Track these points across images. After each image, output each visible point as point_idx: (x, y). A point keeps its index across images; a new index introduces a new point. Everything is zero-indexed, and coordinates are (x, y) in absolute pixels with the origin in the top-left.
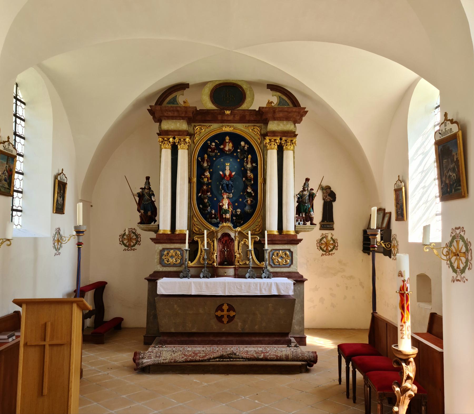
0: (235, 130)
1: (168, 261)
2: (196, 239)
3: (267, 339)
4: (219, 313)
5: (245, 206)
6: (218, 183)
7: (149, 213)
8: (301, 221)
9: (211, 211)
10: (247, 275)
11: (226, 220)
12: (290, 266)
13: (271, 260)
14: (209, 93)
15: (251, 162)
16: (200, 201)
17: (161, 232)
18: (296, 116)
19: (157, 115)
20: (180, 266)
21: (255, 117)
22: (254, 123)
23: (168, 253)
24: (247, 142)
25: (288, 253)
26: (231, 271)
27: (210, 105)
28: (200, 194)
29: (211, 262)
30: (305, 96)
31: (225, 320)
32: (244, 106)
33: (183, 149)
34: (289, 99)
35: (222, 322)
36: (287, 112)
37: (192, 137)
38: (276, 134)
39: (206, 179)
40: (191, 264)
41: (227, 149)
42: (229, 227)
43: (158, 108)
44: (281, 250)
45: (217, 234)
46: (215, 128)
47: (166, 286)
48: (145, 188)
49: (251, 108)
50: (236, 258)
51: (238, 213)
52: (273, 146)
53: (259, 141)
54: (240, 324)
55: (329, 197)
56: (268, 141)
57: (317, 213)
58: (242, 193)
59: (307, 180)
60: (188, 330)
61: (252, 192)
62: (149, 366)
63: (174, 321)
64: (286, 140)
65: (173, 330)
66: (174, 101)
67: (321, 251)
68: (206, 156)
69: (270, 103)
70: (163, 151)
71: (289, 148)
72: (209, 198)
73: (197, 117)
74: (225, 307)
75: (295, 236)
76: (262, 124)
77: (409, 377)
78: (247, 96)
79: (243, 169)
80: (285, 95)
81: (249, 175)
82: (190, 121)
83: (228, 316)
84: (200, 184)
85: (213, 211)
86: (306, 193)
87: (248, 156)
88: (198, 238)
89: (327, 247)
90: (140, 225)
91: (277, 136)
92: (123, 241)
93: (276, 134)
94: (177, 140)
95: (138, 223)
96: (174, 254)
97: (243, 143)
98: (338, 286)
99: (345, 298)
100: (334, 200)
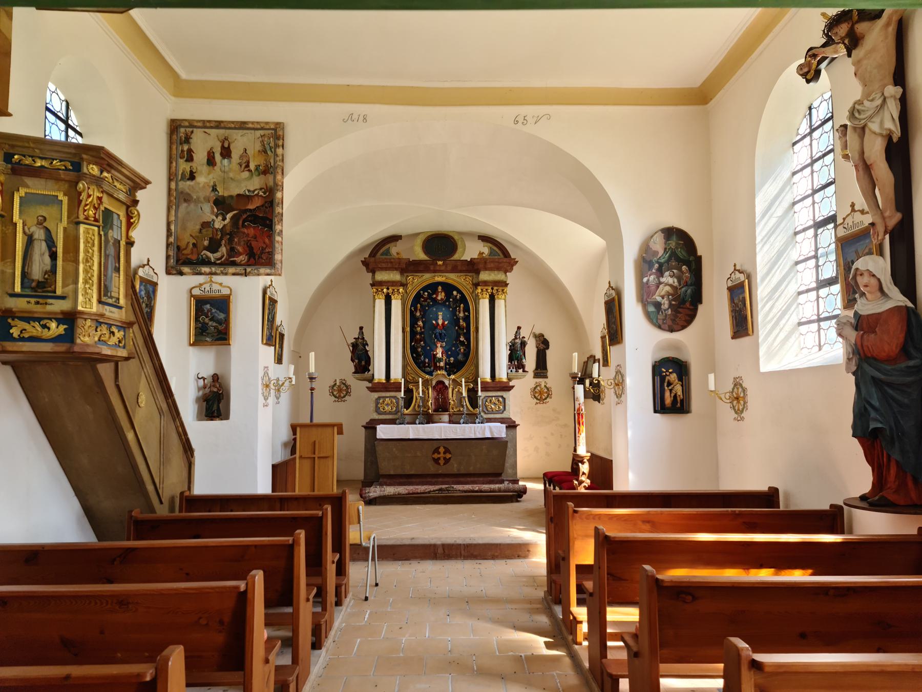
2: (411, 387)
4: (436, 456)
7: (363, 363)
11: (440, 368)
16: (413, 350)
19: (371, 267)
24: (459, 291)
26: (446, 417)
27: (422, 256)
30: (517, 246)
31: (442, 462)
32: (456, 257)
35: (439, 464)
40: (406, 412)
41: (439, 298)
43: (372, 259)
46: (428, 278)
47: (384, 432)
57: (530, 361)
59: (519, 328)
62: (375, 498)
65: (392, 473)
66: (387, 252)
69: (481, 254)
70: (377, 301)
74: (442, 450)
75: (508, 383)
77: (584, 473)
82: (403, 271)
83: (445, 458)
84: (413, 333)
86: (518, 341)
87: (460, 304)
89: (541, 395)
94: (390, 291)
97: (455, 293)
98: (552, 434)
99: (560, 446)
100: (548, 348)
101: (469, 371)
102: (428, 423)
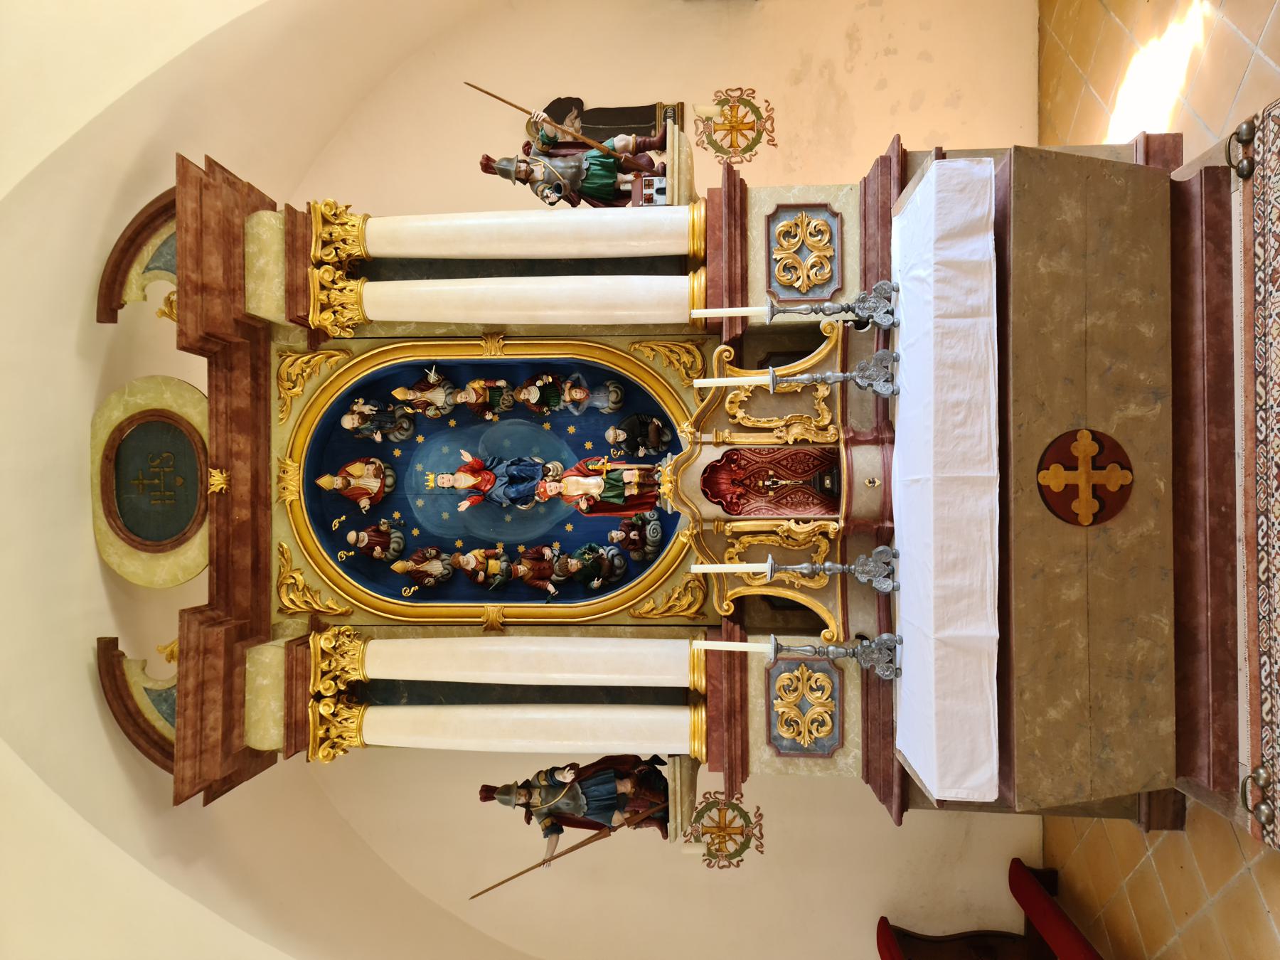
0: (296, 454)
1: (822, 724)
2: (727, 608)
3: (1200, 283)
4: (1085, 506)
5: (593, 410)
6: (508, 518)
7: (625, 787)
8: (650, 185)
9: (616, 545)
10: (882, 388)
11: (649, 483)
12: (835, 215)
13: (811, 296)
14: (144, 555)
15: (422, 390)
16: (574, 587)
17: (699, 749)
18: (217, 197)
20: (841, 671)
21: (237, 373)
22: (267, 378)
23: (789, 723)
24: (343, 405)
25: (780, 226)
26: (861, 462)
27: (194, 553)
28: (551, 588)
29: (824, 545)
31: (1113, 478)
32: (196, 414)
33: (362, 662)
34: (156, 230)
35: (1126, 491)
36: (200, 234)
37: (324, 620)
38: (300, 281)
39: (492, 562)
42: (675, 471)
44: (769, 253)
45: (705, 520)
46: (290, 531)
48: (527, 806)
49: (204, 387)
50: (805, 441)
51: (622, 436)
52: (348, 297)
53: (340, 357)
54: (1133, 410)
55: (567, 121)
56: (326, 319)
58: (547, 426)
59: (488, 165)
60: (1166, 652)
61: (539, 383)
63: (1125, 722)
64: (325, 244)
65: (1167, 725)
67: (757, 148)
68: (398, 566)
71: (355, 232)
72: (566, 552)
73: (239, 605)
74: (1056, 478)
76: (274, 347)
78: (155, 405)
79: (452, 423)
80: (139, 249)
81: (472, 398)
82: (255, 628)
83: (1097, 464)
84: (509, 588)
85: (617, 535)
87: (386, 408)
88: (722, 598)
90: (671, 826)
91: (306, 279)
92: (730, 856)
93: (300, 281)
95: (665, 835)
96: (792, 697)
97: (349, 422)
98: (882, 85)
100: (578, 103)
101: (660, 365)
102: (887, 537)
